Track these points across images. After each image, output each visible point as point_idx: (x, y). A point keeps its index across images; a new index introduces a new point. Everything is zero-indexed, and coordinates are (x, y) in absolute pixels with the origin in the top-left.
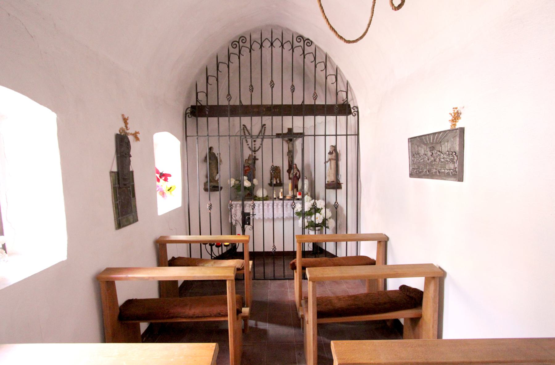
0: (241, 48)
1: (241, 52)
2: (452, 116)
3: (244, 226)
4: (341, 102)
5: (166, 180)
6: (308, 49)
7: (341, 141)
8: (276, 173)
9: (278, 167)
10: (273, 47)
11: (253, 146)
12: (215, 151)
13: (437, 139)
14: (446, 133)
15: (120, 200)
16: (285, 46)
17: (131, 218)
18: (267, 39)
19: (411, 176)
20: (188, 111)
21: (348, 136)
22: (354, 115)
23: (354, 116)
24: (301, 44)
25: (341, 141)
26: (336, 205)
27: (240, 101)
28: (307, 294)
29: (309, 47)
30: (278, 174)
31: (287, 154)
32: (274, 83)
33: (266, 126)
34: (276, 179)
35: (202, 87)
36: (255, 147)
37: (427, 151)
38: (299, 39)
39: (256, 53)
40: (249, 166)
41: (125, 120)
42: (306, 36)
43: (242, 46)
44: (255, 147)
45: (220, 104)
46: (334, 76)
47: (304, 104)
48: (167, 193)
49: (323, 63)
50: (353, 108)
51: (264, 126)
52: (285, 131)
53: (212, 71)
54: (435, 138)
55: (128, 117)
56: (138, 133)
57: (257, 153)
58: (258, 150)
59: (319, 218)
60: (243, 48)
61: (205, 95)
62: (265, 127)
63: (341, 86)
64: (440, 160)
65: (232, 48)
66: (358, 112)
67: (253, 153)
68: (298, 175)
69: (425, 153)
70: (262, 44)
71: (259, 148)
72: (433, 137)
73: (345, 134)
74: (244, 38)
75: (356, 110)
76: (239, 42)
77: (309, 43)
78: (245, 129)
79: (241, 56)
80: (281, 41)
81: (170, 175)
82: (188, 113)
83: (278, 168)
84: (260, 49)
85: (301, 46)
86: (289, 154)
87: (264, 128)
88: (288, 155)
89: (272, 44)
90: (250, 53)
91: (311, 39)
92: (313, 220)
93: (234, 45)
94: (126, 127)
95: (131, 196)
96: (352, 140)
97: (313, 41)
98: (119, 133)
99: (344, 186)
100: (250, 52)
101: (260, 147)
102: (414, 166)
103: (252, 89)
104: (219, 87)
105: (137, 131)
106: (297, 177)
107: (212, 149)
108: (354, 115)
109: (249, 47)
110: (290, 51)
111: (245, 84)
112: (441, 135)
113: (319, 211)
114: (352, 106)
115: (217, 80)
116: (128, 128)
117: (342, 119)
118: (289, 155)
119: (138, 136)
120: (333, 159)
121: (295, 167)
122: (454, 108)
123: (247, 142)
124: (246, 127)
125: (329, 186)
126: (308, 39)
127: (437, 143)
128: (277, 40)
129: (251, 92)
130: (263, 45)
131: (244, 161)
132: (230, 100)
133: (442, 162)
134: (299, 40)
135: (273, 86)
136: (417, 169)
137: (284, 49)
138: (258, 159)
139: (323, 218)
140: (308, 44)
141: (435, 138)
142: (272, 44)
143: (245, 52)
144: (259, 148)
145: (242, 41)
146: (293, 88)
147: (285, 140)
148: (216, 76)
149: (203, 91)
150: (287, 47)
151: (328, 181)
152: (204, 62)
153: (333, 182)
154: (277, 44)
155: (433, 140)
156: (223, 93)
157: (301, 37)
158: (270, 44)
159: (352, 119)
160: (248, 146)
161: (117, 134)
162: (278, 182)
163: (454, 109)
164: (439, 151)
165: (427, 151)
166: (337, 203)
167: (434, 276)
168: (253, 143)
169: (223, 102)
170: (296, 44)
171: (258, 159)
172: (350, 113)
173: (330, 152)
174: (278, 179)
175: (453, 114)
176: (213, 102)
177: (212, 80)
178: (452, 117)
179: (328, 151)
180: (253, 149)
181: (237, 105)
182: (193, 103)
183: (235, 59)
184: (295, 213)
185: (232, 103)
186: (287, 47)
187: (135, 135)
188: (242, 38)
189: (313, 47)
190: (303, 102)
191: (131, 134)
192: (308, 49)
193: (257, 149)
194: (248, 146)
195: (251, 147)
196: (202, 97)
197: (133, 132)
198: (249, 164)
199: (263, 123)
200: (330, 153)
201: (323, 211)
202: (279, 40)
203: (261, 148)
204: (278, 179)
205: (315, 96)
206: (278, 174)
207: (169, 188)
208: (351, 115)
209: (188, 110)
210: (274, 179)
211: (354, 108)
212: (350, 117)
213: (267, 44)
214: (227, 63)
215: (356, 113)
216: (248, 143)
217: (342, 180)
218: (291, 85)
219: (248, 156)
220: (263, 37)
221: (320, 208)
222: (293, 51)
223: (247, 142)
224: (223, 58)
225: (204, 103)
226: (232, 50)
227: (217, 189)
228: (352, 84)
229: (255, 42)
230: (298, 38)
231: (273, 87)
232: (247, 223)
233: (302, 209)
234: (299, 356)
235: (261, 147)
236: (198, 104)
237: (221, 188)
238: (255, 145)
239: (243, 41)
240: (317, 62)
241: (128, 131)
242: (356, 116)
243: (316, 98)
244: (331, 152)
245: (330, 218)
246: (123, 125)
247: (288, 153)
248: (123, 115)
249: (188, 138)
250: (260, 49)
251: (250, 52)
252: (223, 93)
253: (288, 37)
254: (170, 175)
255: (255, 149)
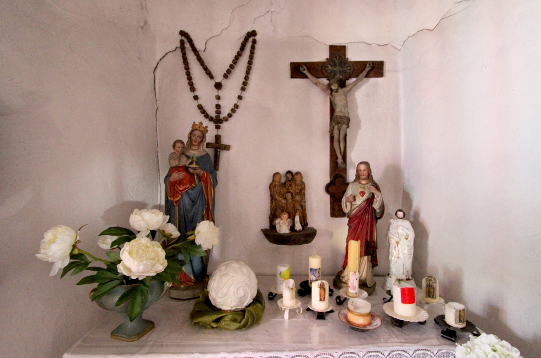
8: (289, 196)
9: (298, 173)
19: (434, 297)
28: (311, 273)
30: (298, 198)
33: (257, 38)
34: (292, 217)
40: (186, 168)
57: (224, 125)
58: (230, 116)
62: (254, 42)
78: (187, 45)
83: (298, 178)
113: (150, 236)
121: (366, 173)
160: (196, 103)
162: (298, 227)
167: (199, 234)
174: (297, 218)
193: (225, 113)
198: (188, 157)
204: (297, 218)
206: (298, 198)
210: (285, 216)
219: (189, 129)
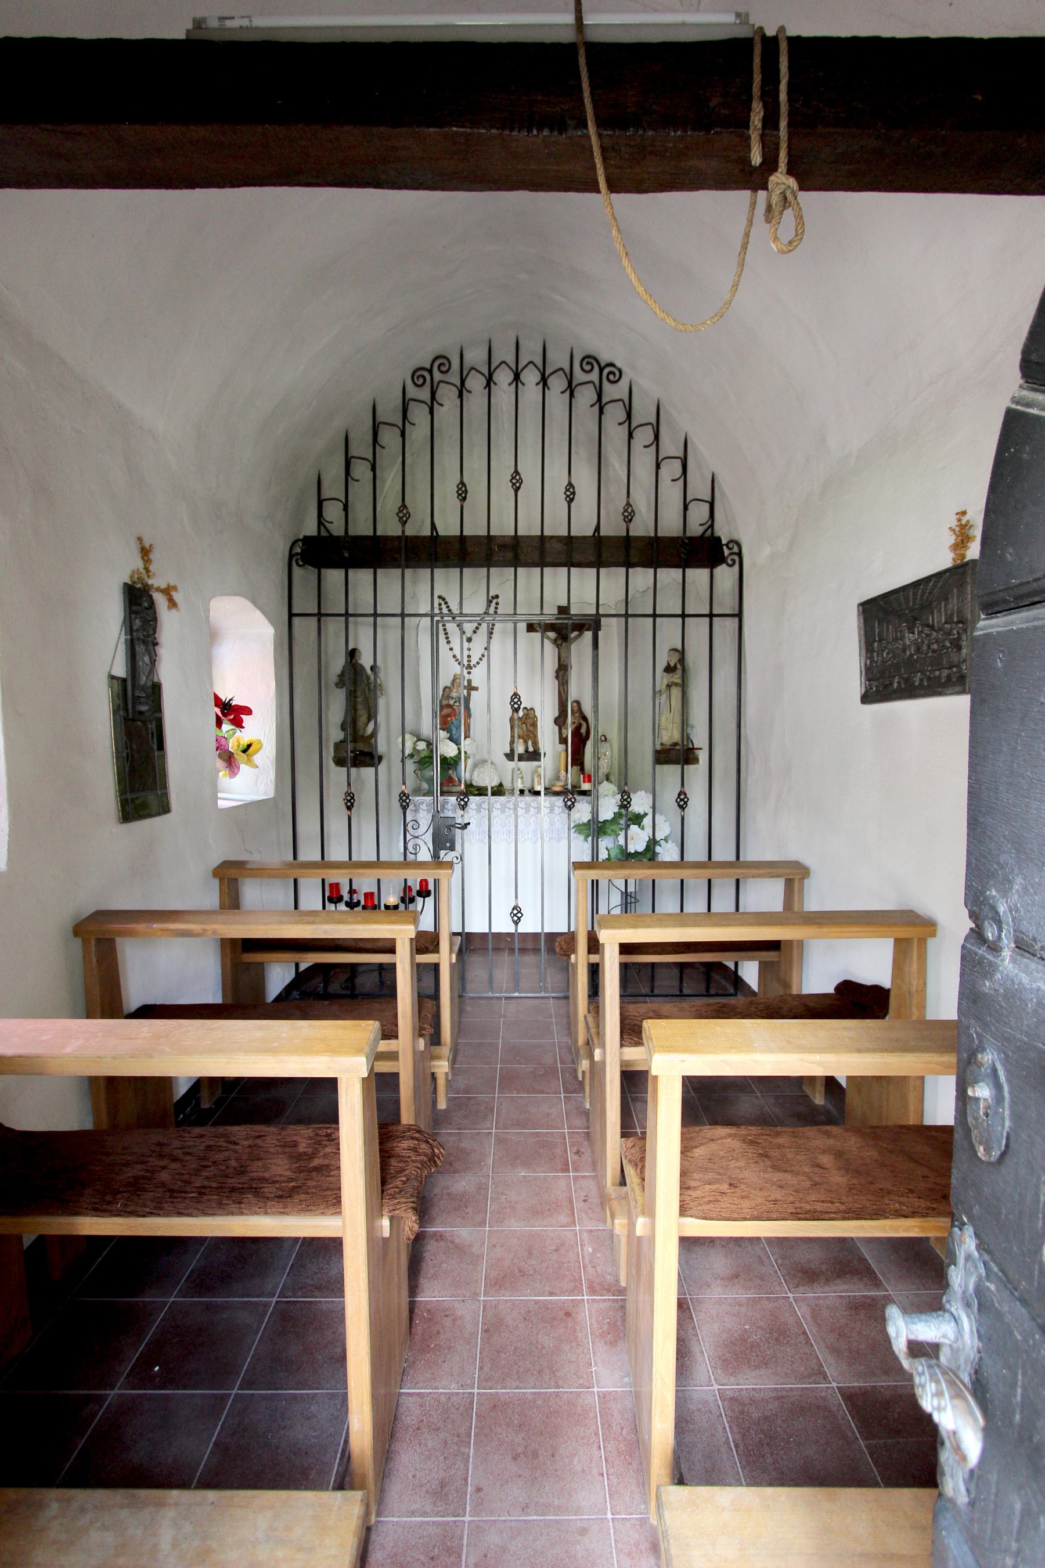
0: (438, 386)
1: (438, 396)
2: (955, 533)
3: (439, 853)
4: (695, 529)
5: (238, 723)
6: (611, 391)
7: (698, 629)
10: (519, 384)
11: (466, 653)
12: (366, 660)
13: (922, 595)
14: (941, 577)
15: (129, 751)
16: (550, 381)
17: (151, 798)
18: (504, 362)
20: (298, 550)
21: (715, 612)
22: (730, 562)
23: (730, 566)
24: (594, 376)
25: (698, 629)
26: (682, 800)
27: (433, 527)
29: (616, 385)
31: (555, 675)
32: (520, 478)
33: (500, 600)
34: (526, 742)
35: (333, 488)
36: (469, 656)
37: (901, 632)
38: (588, 363)
39: (476, 401)
41: (145, 553)
42: (605, 357)
43: (440, 382)
44: (469, 656)
45: (379, 533)
46: (679, 461)
47: (599, 533)
48: (240, 757)
49: (650, 427)
50: (727, 545)
51: (495, 601)
52: (551, 610)
53: (361, 448)
54: (919, 594)
55: (151, 545)
56: (175, 588)
58: (478, 663)
59: (638, 839)
60: (441, 385)
61: (341, 505)
62: (497, 604)
63: (699, 487)
64: (929, 647)
65: (413, 385)
66: (740, 554)
67: (466, 671)
68: (583, 730)
69: (896, 636)
70: (491, 375)
71: (481, 659)
72: (914, 593)
73: (707, 612)
74: (445, 362)
75: (736, 549)
76: (430, 371)
77: (614, 374)
78: (444, 606)
79: (435, 405)
80: (541, 367)
81: (248, 711)
82: (297, 554)
84: (485, 388)
85: (592, 382)
86: (561, 674)
87: (493, 605)
88: (557, 677)
89: (517, 377)
90: (458, 402)
91: (619, 364)
92: (620, 843)
93: (418, 377)
94: (147, 570)
95: (155, 747)
96: (725, 628)
97: (624, 369)
98: (129, 582)
99: (703, 756)
100: (461, 396)
101: (483, 656)
102: (872, 673)
103: (462, 492)
104: (378, 490)
105: (172, 584)
106: (581, 734)
107: (357, 654)
108: (730, 562)
109: (458, 384)
110: (563, 395)
111: (447, 489)
112: (931, 584)
114: (724, 542)
115: (374, 469)
116: (151, 574)
117: (698, 576)
118: (560, 678)
119: (176, 596)
120: (676, 685)
122: (957, 514)
123: (449, 642)
124: (446, 603)
125: (665, 756)
126: (612, 365)
127: (923, 607)
128: (531, 365)
129: (461, 500)
130: (495, 378)
131: (441, 693)
132: (406, 522)
133: (934, 651)
134: (588, 368)
135: (518, 485)
136: (878, 679)
137: (549, 389)
138: (476, 689)
139: (647, 839)
140: (611, 377)
141: (919, 594)
142: (517, 377)
143: (448, 395)
144: (481, 659)
145: (439, 367)
146: (571, 490)
147: (548, 638)
148: (371, 458)
149: (337, 497)
150: (557, 384)
151: (662, 744)
152: (339, 424)
153: (676, 744)
154: (531, 377)
155: (915, 599)
156: (389, 502)
157: (590, 360)
158: (512, 376)
159: (725, 575)
160: (451, 653)
161: (125, 584)
162: (531, 749)
163: (958, 516)
164: (928, 626)
165: (901, 632)
166: (685, 794)
168: (466, 645)
169: (389, 527)
170: (579, 376)
171: (476, 689)
172: (722, 560)
173: (669, 665)
174: (530, 743)
175: (957, 529)
176: (361, 527)
177: (362, 470)
178: (954, 537)
179: (661, 665)
180: (466, 663)
181: (425, 537)
182: (310, 529)
183: (419, 414)
184: (574, 827)
185: (410, 532)
186: (557, 384)
187: (167, 591)
188: (441, 361)
189: (624, 384)
190: (598, 529)
191: (158, 590)
192: (611, 391)
194: (451, 653)
195: (459, 657)
196: (333, 513)
197: (163, 586)
199: (492, 593)
200: (669, 669)
201: (647, 821)
202: (535, 365)
203: (485, 659)
204: (530, 743)
205: (630, 514)
207: (245, 747)
208: (724, 566)
209: (297, 544)
211: (731, 546)
212: (721, 571)
213: (503, 377)
214: (400, 424)
215: (736, 558)
216: (451, 645)
217: (699, 738)
218: (566, 483)
219: (452, 678)
220: (493, 360)
221: (642, 813)
222: (572, 395)
223: (449, 642)
224: (389, 411)
225: (337, 529)
226: (412, 392)
227: (368, 759)
228: (725, 484)
229: (473, 372)
230: (585, 363)
231: (519, 488)
232: (448, 845)
233: (593, 816)
234: (576, 1157)
235: (486, 654)
236: (324, 533)
237: (380, 758)
238: (469, 649)
239: (444, 369)
240: (633, 426)
241: (150, 582)
242: (736, 567)
243: (632, 517)
244: (672, 665)
245: (666, 840)
246: (140, 564)
247: (557, 672)
248: (140, 539)
249: (296, 620)
250: (487, 389)
251: (461, 396)
252: (389, 502)
253: (558, 359)
254: (248, 711)
255: (469, 661)
